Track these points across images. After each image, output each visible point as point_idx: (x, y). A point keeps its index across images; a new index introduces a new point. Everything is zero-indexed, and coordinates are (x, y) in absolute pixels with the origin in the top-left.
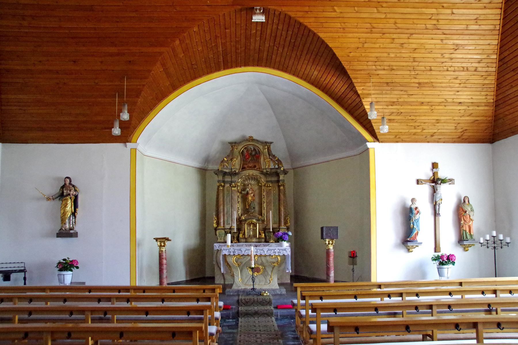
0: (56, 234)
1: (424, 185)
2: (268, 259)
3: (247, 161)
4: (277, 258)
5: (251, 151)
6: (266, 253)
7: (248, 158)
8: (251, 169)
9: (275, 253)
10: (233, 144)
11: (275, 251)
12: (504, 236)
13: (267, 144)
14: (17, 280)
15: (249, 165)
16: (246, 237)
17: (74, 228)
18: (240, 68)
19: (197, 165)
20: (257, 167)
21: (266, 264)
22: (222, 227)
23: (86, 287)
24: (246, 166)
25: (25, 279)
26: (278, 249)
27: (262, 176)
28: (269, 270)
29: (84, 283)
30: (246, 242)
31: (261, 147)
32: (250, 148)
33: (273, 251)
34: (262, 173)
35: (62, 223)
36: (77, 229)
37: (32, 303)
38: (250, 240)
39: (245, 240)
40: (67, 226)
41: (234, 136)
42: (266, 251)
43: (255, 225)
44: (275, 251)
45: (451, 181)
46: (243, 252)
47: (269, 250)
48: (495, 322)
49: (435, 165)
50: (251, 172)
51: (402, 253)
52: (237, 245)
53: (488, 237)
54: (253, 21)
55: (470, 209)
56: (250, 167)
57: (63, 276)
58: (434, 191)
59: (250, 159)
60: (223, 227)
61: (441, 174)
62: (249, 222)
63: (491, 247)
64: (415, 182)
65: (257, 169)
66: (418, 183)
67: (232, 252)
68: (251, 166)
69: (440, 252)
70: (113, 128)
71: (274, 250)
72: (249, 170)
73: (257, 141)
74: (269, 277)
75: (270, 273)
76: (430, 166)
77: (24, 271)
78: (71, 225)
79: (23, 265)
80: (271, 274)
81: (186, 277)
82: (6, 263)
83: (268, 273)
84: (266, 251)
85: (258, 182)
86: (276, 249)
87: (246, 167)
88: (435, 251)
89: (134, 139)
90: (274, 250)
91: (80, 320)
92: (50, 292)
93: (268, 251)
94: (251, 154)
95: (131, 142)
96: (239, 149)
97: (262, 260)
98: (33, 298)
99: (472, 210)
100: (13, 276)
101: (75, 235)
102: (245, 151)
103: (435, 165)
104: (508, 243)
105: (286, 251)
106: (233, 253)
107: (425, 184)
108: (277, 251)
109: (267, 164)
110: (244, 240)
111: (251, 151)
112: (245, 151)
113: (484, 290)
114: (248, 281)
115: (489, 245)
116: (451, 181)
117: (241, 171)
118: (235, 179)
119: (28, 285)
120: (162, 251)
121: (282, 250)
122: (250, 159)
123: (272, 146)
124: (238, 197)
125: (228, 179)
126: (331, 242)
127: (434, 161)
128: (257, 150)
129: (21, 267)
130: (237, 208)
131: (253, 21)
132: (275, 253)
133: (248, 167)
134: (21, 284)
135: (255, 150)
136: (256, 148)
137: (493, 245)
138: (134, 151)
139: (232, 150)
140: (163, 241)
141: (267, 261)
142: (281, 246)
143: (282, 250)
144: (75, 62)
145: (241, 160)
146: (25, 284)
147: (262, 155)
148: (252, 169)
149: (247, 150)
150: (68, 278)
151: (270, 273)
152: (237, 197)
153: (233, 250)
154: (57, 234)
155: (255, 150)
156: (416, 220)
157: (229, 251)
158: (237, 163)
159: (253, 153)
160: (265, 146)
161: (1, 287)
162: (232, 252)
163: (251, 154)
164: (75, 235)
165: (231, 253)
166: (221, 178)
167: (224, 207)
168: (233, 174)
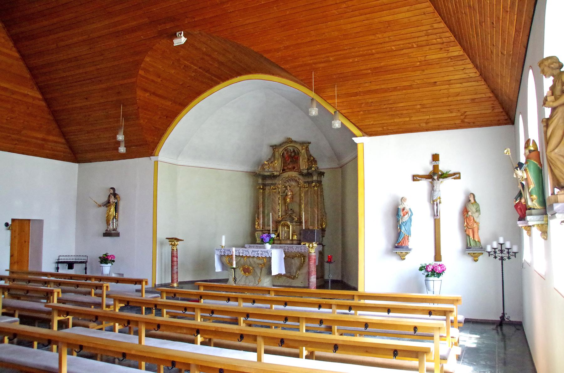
0: (102, 234)
1: (420, 181)
2: (255, 261)
3: (287, 163)
4: (263, 260)
5: (291, 152)
6: (250, 254)
7: (288, 160)
8: (290, 171)
9: (258, 254)
10: (274, 147)
11: (258, 252)
12: (512, 245)
13: (306, 144)
14: (77, 270)
15: (289, 167)
16: (280, 239)
17: (116, 229)
18: (237, 78)
19: (247, 168)
20: (296, 169)
21: (254, 265)
22: (261, 229)
23: (125, 279)
24: (286, 168)
25: (86, 269)
26: (261, 251)
27: (301, 177)
28: (258, 271)
29: (123, 275)
30: (280, 244)
31: (300, 148)
32: (290, 150)
33: (256, 253)
34: (301, 174)
35: (107, 224)
36: (119, 230)
37: (60, 286)
38: (283, 242)
39: (279, 241)
40: (111, 227)
41: (277, 140)
42: (250, 253)
43: (289, 227)
44: (258, 252)
45: (456, 176)
46: (250, 254)
47: (253, 251)
48: (392, 349)
49: (435, 157)
50: (294, 174)
51: (394, 260)
52: (250, 246)
53: (495, 245)
54: (174, 45)
55: (474, 210)
56: (290, 169)
57: (102, 267)
58: (432, 189)
59: (290, 160)
60: (262, 228)
61: (443, 167)
62: (283, 224)
63: (499, 258)
64: (411, 178)
65: (296, 170)
66: (414, 180)
67: (223, 252)
68: (290, 167)
69: (441, 261)
70: (120, 147)
71: (257, 252)
72: (289, 171)
73: (295, 142)
74: (258, 278)
75: (259, 275)
76: (430, 158)
77: (85, 262)
78: (115, 227)
79: (85, 258)
80: (260, 275)
81: (105, 274)
82: (69, 256)
83: (257, 274)
84: (250, 253)
85: (298, 182)
86: (258, 251)
87: (286, 169)
88: (436, 260)
89: (156, 153)
90: (257, 252)
91: (224, 305)
92: (95, 281)
93: (252, 252)
94: (291, 155)
95: (154, 156)
96: (280, 152)
97: (250, 261)
98: (80, 284)
99: (478, 211)
100: (75, 266)
101: (118, 235)
102: (285, 153)
103: (435, 157)
104: (515, 253)
105: (268, 253)
106: (224, 253)
107: (421, 180)
108: (260, 252)
109: (303, 165)
110: (279, 242)
111: (291, 152)
112: (285, 153)
113: (390, 308)
114: (239, 280)
115: (497, 255)
116: (456, 176)
117: (281, 173)
118: (276, 181)
119: (89, 274)
120: (174, 249)
121: (265, 252)
122: (290, 160)
123: (310, 147)
124: (279, 199)
125: (268, 182)
126: (311, 246)
127: (434, 153)
128: (296, 151)
129: (83, 259)
130: (278, 209)
131: (174, 45)
132: (258, 254)
133: (288, 168)
134: (83, 274)
135: (294, 151)
136: (295, 150)
137: (500, 255)
138: (156, 162)
139: (274, 152)
140: (173, 240)
141: (255, 262)
142: (264, 248)
143: (265, 252)
144: (86, 99)
145: (282, 162)
146: (86, 273)
147: (301, 156)
148: (292, 171)
149: (287, 152)
150: (107, 269)
151: (259, 275)
152: (278, 198)
153: (224, 251)
154: (104, 234)
155: (294, 151)
156: (404, 222)
157: (221, 251)
158: (278, 164)
159: (293, 154)
160: (303, 146)
161: (1, 276)
162: (303, 249)
163: (291, 155)
164: (118, 235)
165: (240, 253)
166: (260, 181)
167: (264, 207)
168: (273, 177)
